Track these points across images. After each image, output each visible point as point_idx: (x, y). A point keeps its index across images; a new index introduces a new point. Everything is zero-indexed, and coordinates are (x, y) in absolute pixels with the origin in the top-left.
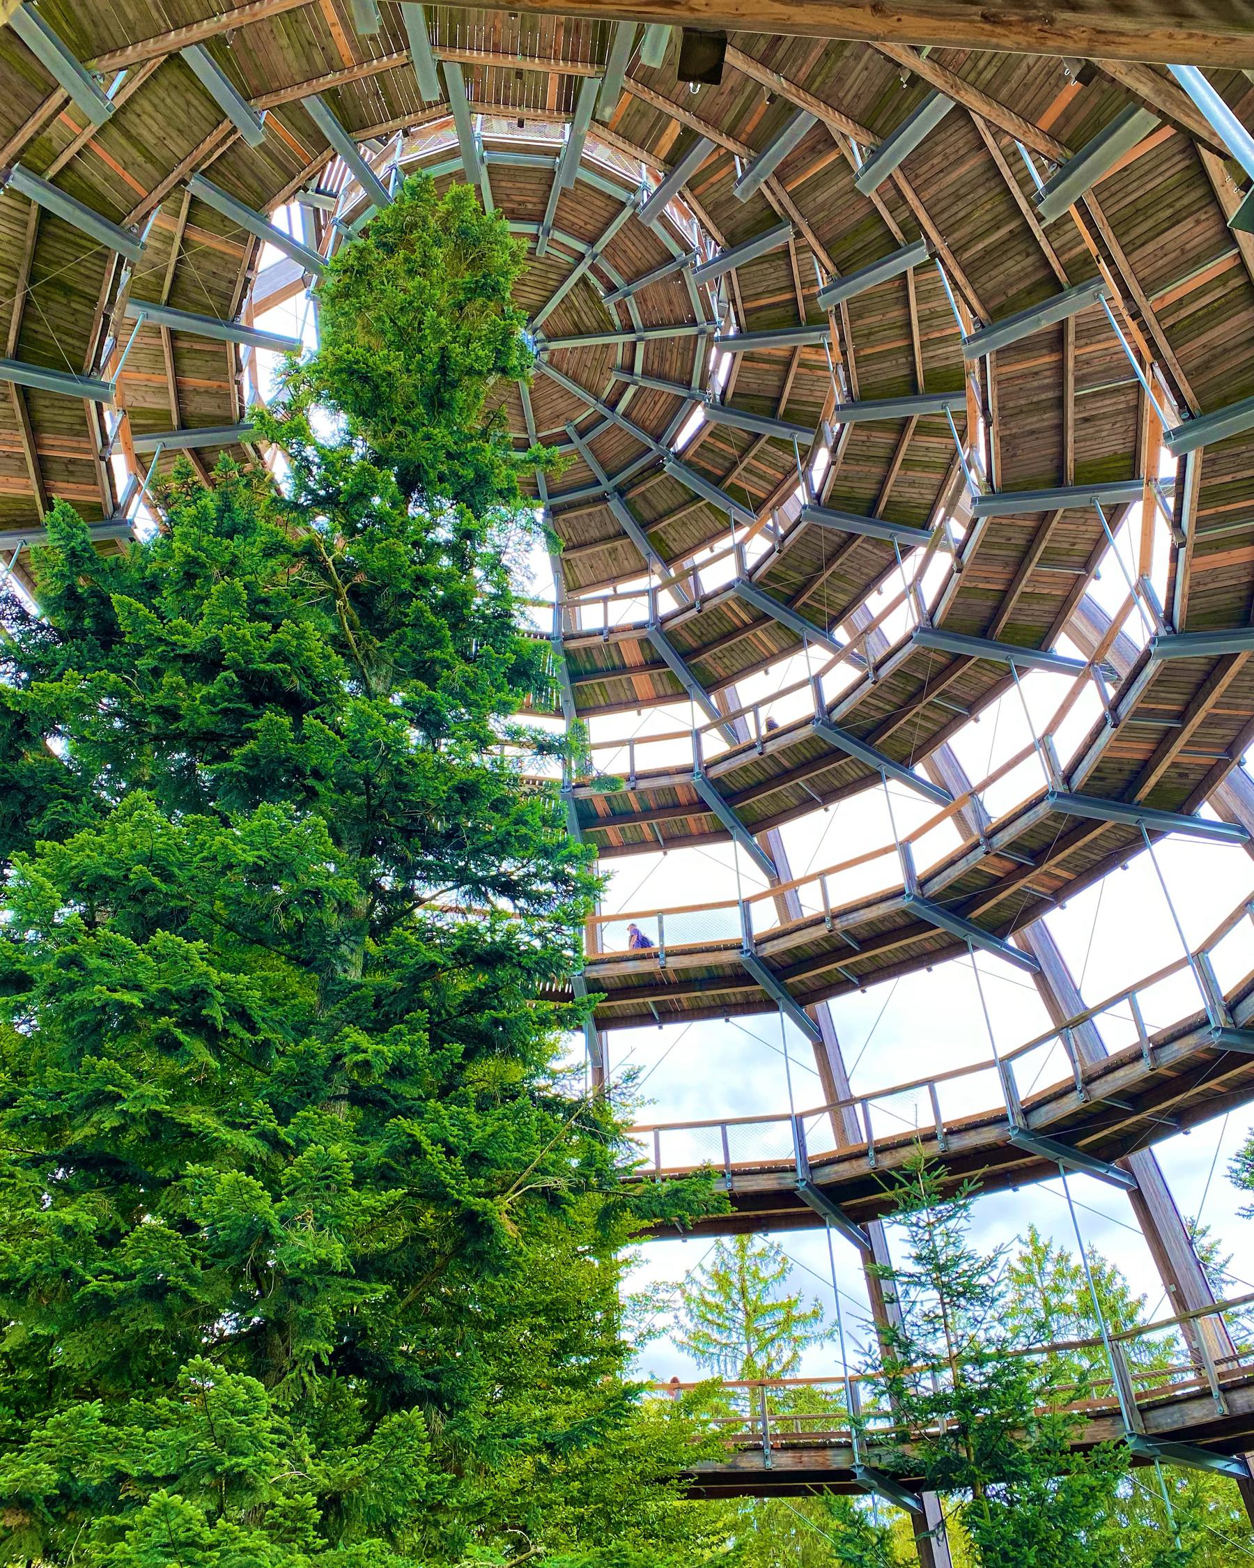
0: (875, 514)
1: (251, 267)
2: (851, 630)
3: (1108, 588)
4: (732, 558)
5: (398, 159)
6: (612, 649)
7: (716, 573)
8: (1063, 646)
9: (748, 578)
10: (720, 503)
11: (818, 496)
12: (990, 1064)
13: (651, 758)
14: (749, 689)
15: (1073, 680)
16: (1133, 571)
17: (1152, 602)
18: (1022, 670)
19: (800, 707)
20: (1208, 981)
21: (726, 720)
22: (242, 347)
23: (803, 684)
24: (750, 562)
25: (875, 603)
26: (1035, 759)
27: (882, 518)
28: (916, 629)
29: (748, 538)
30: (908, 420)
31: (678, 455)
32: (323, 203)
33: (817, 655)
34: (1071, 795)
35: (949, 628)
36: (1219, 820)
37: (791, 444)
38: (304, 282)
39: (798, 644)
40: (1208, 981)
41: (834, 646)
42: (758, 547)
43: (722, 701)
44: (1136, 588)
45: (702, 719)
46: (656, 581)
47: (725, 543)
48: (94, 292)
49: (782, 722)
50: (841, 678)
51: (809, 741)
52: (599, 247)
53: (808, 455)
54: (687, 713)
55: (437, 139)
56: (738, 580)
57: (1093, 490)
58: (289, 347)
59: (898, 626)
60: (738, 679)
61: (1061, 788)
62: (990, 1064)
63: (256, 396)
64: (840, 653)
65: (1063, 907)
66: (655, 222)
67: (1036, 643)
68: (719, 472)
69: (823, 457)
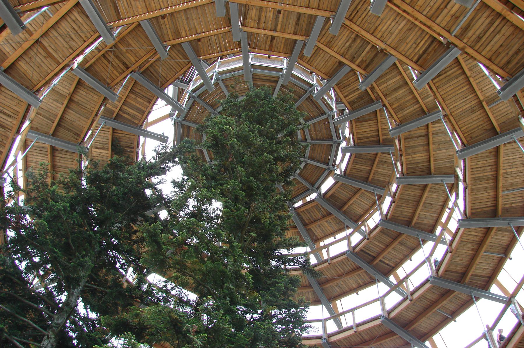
0: (407, 229)
1: (152, 108)
2: (396, 277)
4: (345, 242)
5: (217, 70)
6: (473, 170)
7: (374, 220)
9: (353, 251)
10: (342, 217)
13: (362, 315)
14: (345, 303)
18: (477, 299)
21: (335, 316)
22: (141, 137)
23: (424, 262)
25: (408, 266)
27: (413, 227)
28: (431, 277)
29: (351, 234)
31: (295, 209)
32: (182, 86)
33: (381, 288)
35: (394, 321)
37: (374, 193)
38: (170, 115)
39: (372, 282)
41: (388, 284)
42: (356, 238)
43: (396, 277)
45: (327, 315)
46: (309, 249)
47: (339, 236)
48: (54, 119)
49: (439, 259)
50: (394, 299)
51: (379, 326)
53: (381, 198)
54: (380, 288)
55: (235, 63)
56: (348, 251)
58: (162, 139)
63: (144, 158)
66: (320, 100)
68: (307, 221)
69: (388, 200)
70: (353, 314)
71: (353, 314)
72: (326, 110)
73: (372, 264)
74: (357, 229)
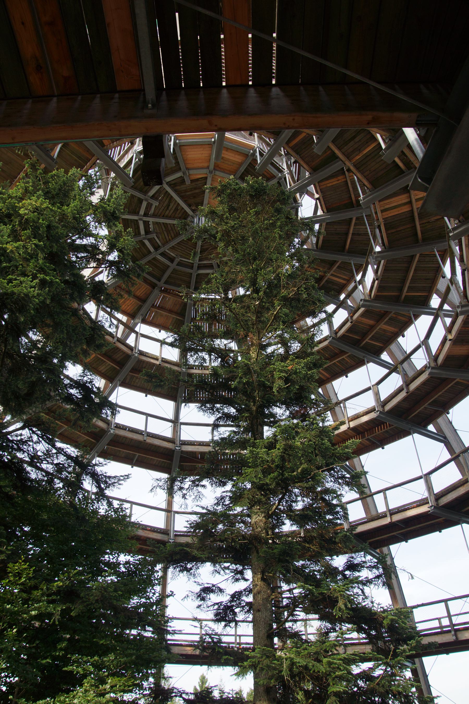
3: (409, 339)
8: (385, 356)
11: (336, 332)
12: (420, 478)
15: (387, 371)
16: (423, 338)
17: (428, 350)
19: (368, 401)
20: (429, 487)
24: (336, 325)
26: (370, 394)
30: (351, 219)
33: (424, 321)
34: (436, 367)
36: (435, 431)
40: (429, 487)
41: (383, 364)
44: (422, 342)
52: (135, 218)
57: (366, 354)
59: (420, 360)
60: (173, 362)
61: (433, 364)
62: (420, 478)
64: (437, 314)
65: (383, 448)
67: (373, 354)
70: (385, 498)
71: (385, 498)
72: (274, 171)
73: (366, 341)
74: (341, 305)
